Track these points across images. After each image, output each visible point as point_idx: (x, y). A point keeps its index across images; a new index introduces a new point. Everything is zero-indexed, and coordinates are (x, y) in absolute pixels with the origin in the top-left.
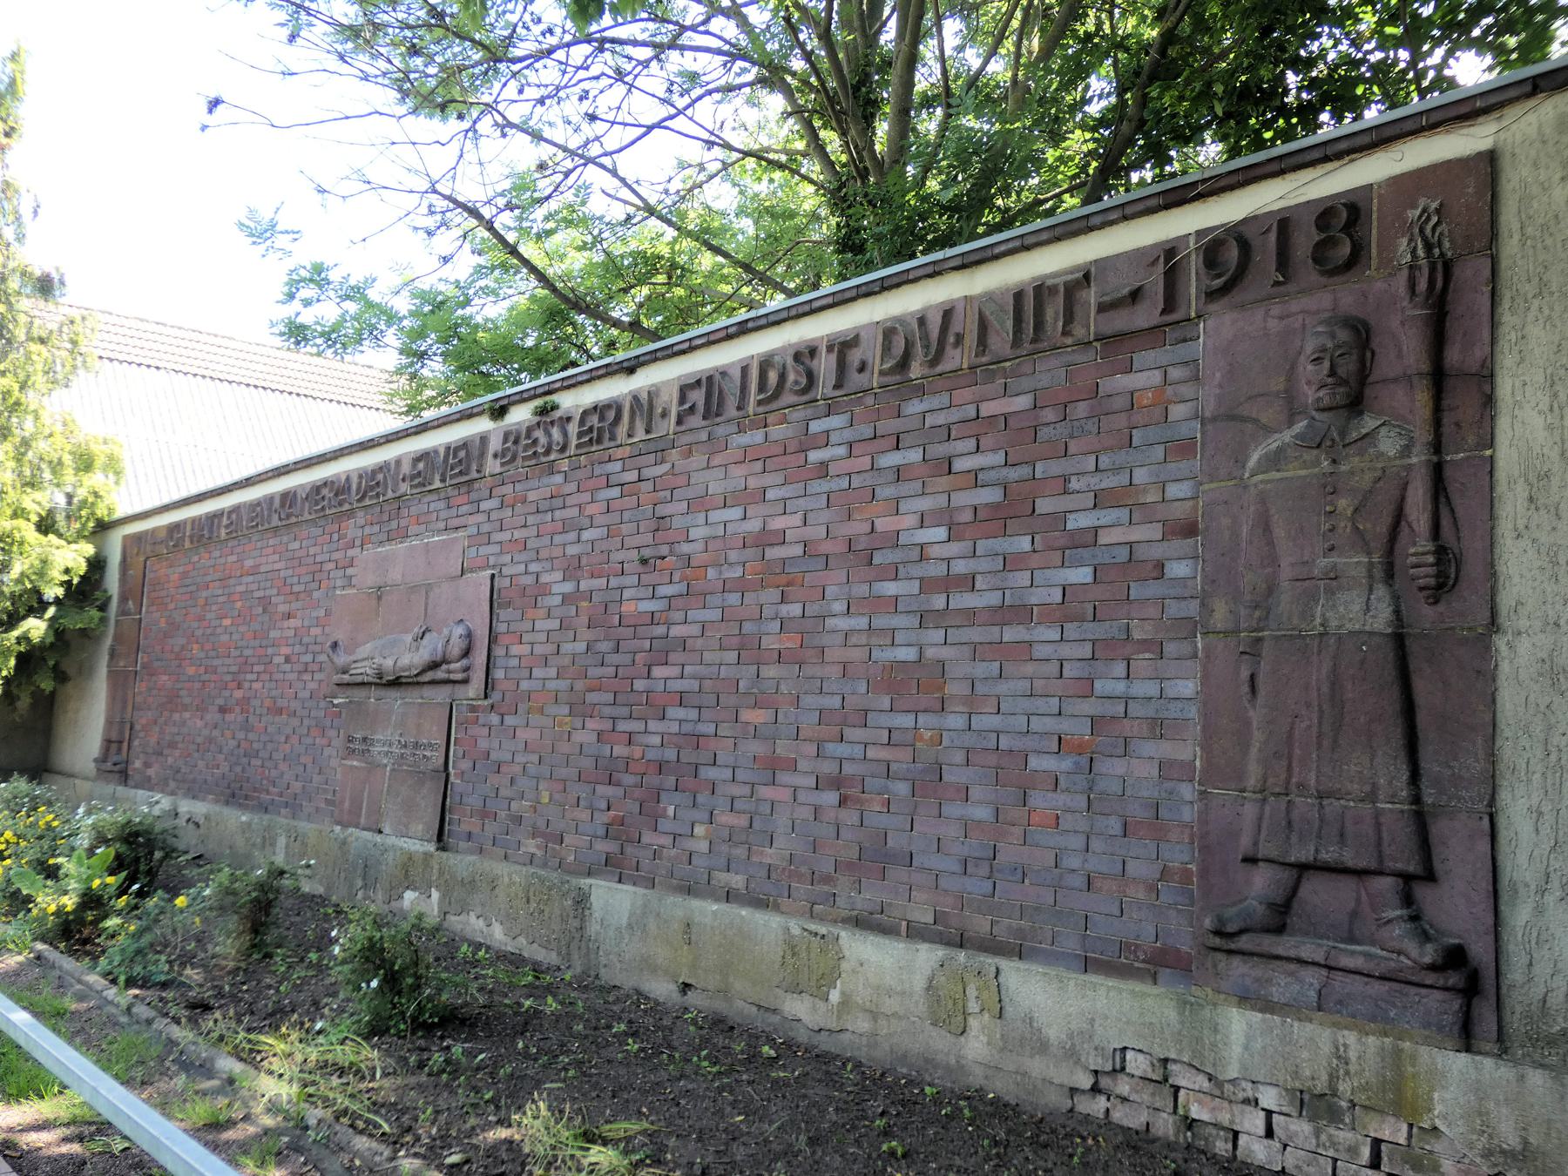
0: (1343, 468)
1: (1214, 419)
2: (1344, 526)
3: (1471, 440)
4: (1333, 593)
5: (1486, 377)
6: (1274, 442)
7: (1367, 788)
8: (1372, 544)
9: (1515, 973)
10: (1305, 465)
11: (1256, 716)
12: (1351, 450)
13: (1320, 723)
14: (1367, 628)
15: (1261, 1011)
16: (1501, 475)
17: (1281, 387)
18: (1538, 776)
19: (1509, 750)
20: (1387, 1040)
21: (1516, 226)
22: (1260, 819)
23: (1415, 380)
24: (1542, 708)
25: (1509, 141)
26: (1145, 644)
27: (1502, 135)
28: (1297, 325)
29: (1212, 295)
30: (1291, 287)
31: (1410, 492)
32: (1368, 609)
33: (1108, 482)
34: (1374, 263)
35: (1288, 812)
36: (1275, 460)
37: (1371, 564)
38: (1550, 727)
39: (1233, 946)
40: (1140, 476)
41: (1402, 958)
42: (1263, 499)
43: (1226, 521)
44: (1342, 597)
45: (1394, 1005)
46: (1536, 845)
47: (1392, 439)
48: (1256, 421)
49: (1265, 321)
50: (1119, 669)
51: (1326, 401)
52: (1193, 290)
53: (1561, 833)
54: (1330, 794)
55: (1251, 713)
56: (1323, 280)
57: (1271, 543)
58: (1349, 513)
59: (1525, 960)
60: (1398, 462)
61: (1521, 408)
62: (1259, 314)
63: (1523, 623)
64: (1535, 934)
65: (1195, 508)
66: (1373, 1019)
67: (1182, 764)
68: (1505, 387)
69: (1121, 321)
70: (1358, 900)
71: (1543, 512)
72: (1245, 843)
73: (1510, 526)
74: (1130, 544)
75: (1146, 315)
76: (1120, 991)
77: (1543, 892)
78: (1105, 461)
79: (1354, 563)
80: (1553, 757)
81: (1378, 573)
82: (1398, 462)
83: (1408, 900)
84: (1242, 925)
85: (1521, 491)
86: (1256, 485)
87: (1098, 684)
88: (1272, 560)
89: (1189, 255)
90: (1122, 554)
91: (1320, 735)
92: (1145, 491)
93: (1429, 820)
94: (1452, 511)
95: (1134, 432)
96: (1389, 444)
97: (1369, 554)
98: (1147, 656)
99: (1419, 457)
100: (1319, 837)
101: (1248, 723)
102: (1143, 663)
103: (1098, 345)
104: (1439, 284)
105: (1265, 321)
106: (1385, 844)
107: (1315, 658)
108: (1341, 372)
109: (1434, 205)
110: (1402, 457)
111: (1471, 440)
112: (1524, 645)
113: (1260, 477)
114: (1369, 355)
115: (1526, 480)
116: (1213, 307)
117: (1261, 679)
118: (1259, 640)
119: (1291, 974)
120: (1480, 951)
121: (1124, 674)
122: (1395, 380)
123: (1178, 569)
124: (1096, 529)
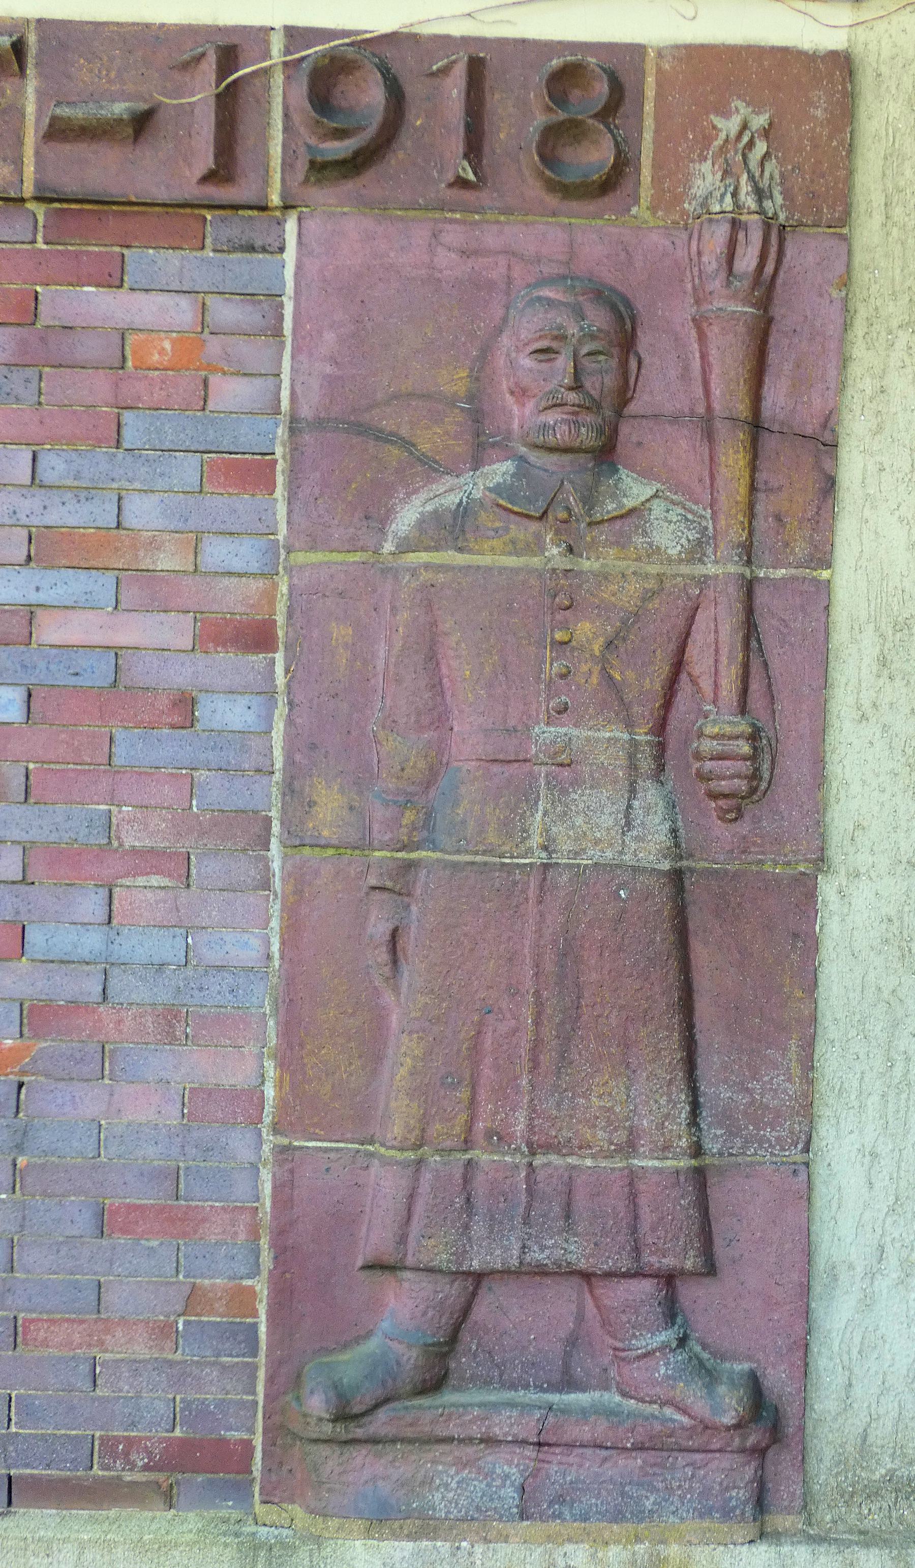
0: (586, 565)
1: (319, 424)
2: (588, 673)
3: (800, 549)
4: (564, 792)
5: (824, 443)
6: (448, 494)
7: (621, 1136)
8: (636, 709)
9: (825, 1402)
10: (515, 549)
11: (403, 1007)
12: (603, 534)
13: (537, 1023)
14: (627, 858)
15: (410, 1537)
16: (841, 616)
17: (461, 388)
18: (875, 1098)
19: (831, 1061)
20: (640, 1548)
21: (878, 199)
22: (412, 1197)
23: (722, 428)
24: (886, 994)
25: (873, 47)
26: (148, 860)
27: (862, 34)
28: (494, 275)
29: (322, 170)
30: (484, 197)
31: (702, 620)
32: (628, 824)
33: (64, 514)
34: (646, 193)
35: (466, 1180)
36: (454, 527)
37: (634, 744)
38: (895, 1024)
39: (359, 1433)
40: (143, 512)
41: (668, 1411)
42: (428, 597)
43: (341, 632)
44: (579, 797)
45: (654, 1489)
46: (866, 1206)
47: (666, 525)
48: (407, 444)
49: (431, 251)
50: (90, 905)
51: (562, 435)
52: (276, 150)
53: (903, 1184)
54: (549, 1147)
55: (389, 998)
56: (553, 201)
57: (437, 687)
58: (596, 649)
59: (841, 1379)
60: (685, 569)
61: (874, 507)
62: (421, 235)
63: (863, 860)
64: (857, 1340)
65: (270, 596)
66: (617, 1517)
67: (234, 1095)
68: (854, 466)
69: (100, 169)
70: (580, 1318)
71: (898, 683)
72: (376, 1238)
73: (851, 700)
74: (117, 651)
75: (176, 167)
76: (110, 1546)
77: (871, 1275)
78: (55, 466)
79: (604, 740)
80: (898, 1071)
81: (646, 764)
82: (685, 569)
83: (671, 1312)
84: (380, 1393)
85: (869, 647)
86: (414, 572)
87: (34, 936)
88: (438, 718)
89: (266, 71)
90: (100, 672)
91: (537, 1045)
92: (154, 545)
93: (712, 1180)
94: (766, 665)
95: (128, 417)
96: (668, 533)
97: (630, 725)
98: (155, 880)
99: (722, 567)
100: (527, 1220)
101: (379, 1019)
102: (145, 891)
103: (40, 211)
104: (769, 268)
105: (431, 251)
106: (645, 1227)
107: (531, 908)
108: (591, 384)
109: (760, 121)
110: (690, 560)
111: (800, 549)
112: (862, 894)
113: (424, 557)
114: (633, 364)
115: (877, 629)
116: (324, 196)
117: (409, 942)
118: (410, 866)
119: (462, 1464)
120: (777, 1379)
121: (102, 916)
122: (675, 419)
123: (227, 713)
124: (30, 613)
